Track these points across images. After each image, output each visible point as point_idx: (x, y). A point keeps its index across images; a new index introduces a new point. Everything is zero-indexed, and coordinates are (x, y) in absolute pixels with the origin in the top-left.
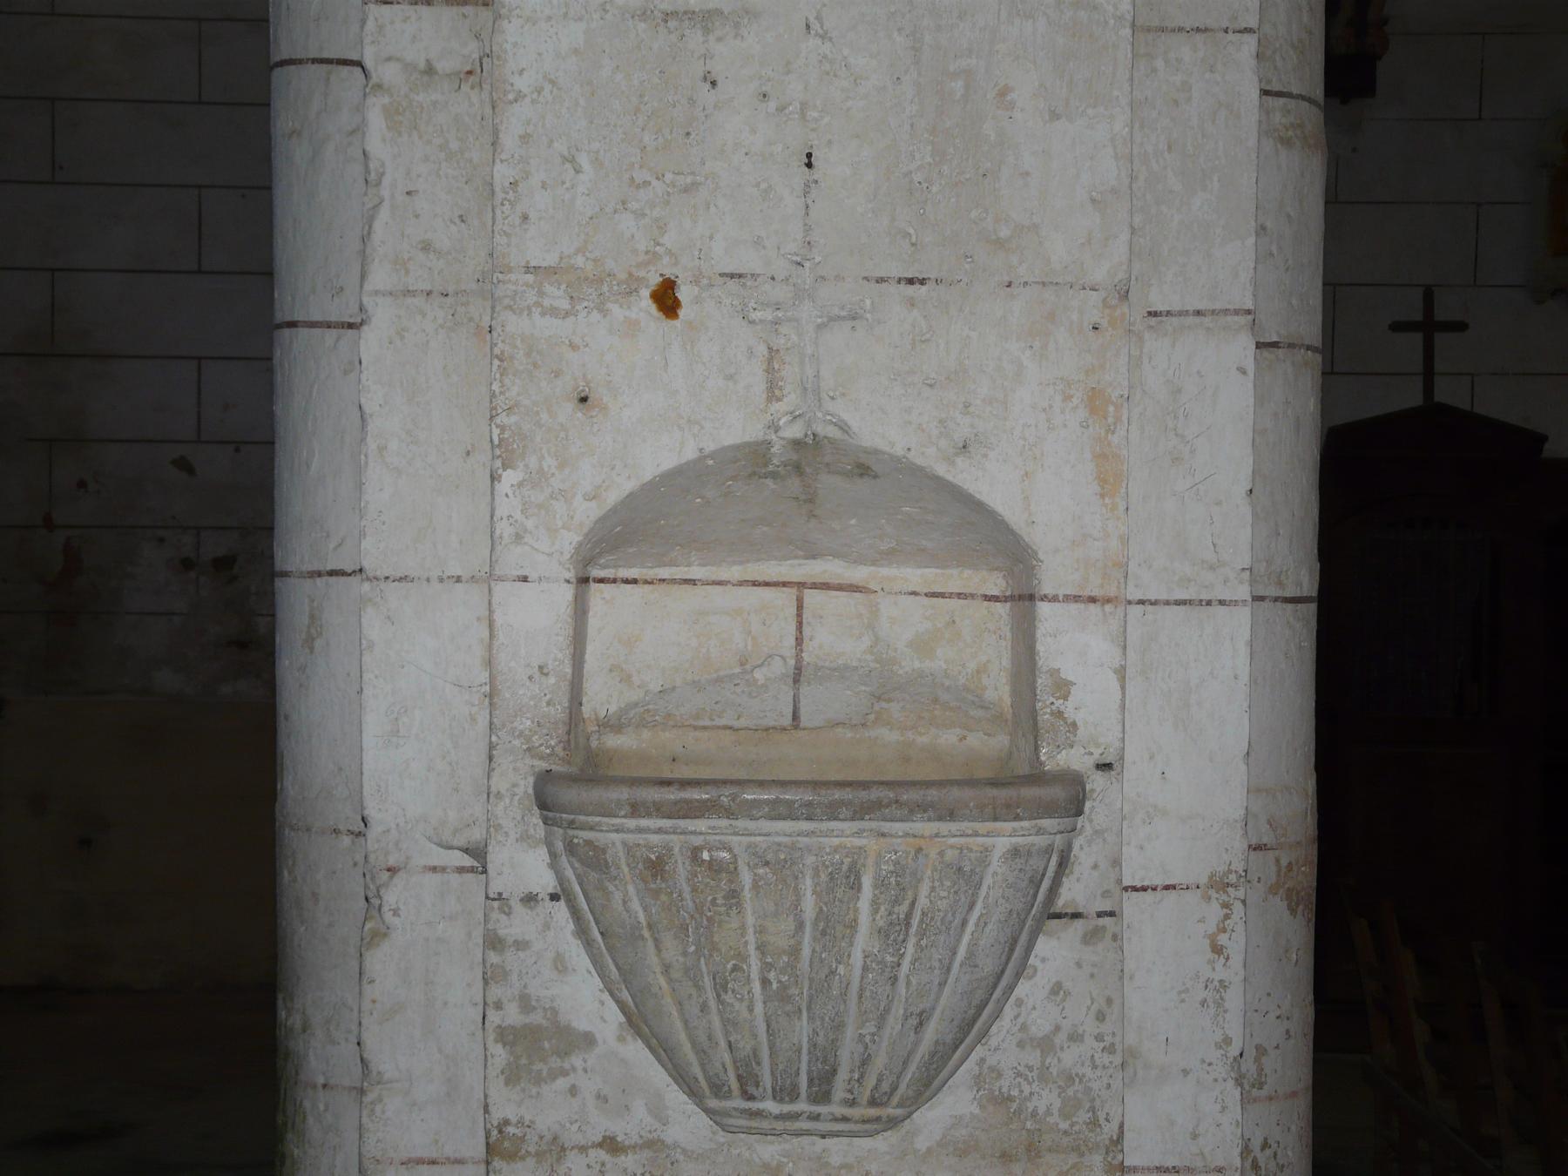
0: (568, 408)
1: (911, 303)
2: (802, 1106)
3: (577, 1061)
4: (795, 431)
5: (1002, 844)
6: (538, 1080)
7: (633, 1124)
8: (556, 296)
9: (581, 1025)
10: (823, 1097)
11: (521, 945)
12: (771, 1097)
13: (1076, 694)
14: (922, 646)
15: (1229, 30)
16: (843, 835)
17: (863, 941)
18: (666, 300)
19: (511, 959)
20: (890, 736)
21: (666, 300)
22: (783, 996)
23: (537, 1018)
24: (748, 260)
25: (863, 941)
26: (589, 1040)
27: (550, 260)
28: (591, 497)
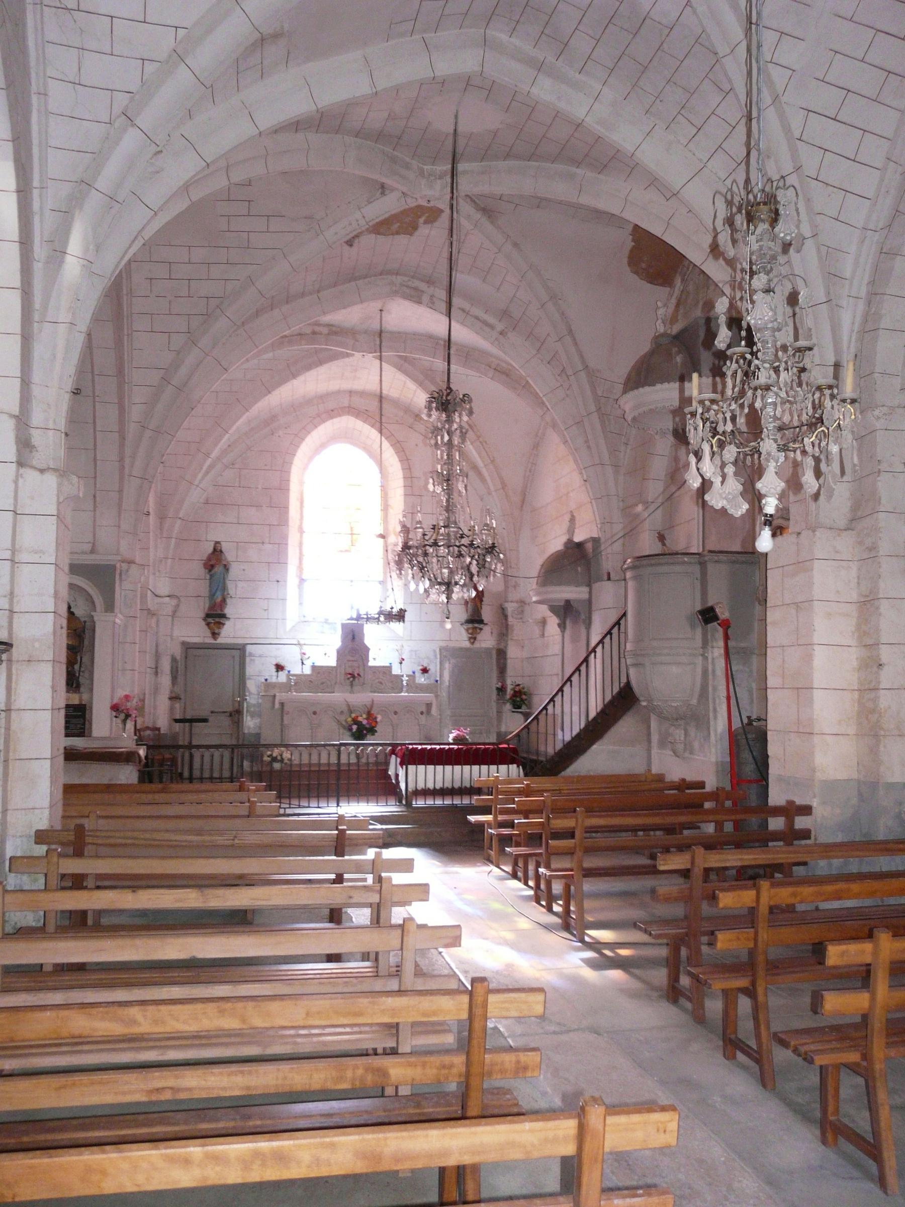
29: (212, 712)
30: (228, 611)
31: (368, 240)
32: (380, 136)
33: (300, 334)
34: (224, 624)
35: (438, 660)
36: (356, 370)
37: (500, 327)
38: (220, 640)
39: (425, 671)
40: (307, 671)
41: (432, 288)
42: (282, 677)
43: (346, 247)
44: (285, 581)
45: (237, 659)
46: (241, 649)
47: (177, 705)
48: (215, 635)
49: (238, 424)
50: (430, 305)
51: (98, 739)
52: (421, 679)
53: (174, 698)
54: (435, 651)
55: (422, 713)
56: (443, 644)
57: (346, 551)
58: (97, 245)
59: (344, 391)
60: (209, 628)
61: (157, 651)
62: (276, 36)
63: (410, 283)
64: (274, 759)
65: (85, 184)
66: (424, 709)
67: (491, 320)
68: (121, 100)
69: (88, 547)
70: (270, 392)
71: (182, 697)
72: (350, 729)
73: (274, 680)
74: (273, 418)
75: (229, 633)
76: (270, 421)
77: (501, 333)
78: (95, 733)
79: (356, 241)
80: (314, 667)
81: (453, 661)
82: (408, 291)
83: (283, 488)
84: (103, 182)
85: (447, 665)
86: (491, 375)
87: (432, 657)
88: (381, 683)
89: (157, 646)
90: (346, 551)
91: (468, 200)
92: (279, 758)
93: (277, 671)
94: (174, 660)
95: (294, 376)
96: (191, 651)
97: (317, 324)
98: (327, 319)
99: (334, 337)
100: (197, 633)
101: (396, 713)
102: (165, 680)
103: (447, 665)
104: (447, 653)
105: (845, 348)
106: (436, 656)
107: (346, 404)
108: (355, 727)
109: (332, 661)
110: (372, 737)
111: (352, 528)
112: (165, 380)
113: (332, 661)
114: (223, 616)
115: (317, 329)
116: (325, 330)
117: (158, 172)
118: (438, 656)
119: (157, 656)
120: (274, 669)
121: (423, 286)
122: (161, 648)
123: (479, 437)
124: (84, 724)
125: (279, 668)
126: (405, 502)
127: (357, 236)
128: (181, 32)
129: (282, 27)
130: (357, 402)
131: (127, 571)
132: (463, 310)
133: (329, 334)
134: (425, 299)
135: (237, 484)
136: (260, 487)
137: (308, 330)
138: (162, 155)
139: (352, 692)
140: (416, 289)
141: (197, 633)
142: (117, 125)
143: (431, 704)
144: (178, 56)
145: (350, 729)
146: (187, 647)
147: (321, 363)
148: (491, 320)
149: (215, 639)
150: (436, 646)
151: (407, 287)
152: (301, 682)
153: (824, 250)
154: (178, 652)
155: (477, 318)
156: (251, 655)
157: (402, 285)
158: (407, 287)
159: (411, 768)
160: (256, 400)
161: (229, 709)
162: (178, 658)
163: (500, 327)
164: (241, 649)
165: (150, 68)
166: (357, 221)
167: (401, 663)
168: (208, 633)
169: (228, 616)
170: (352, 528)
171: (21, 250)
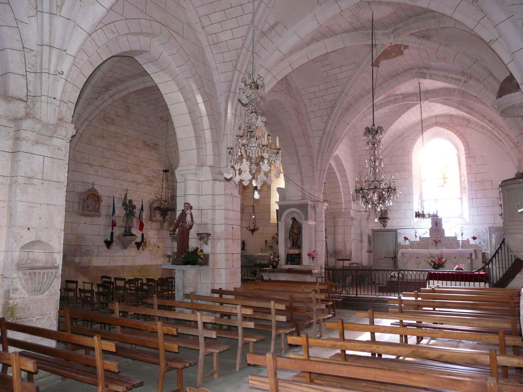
0: (20, 238)
1: (47, 230)
2: (38, 293)
3: (18, 291)
4: (37, 240)
5: (55, 271)
6: (15, 293)
7: (23, 296)
8: (20, 228)
9: (19, 288)
10: (40, 292)
11: (14, 282)
12: (313, 219)
13: (57, 260)
14: (38, 257)
15: (316, 301)
16: (44, 271)
17: (45, 279)
18: (29, 229)
19: (13, 283)
20: (33, 264)
21: (29, 229)
22: (39, 284)
23: (15, 288)
24: (35, 226)
25: (45, 279)
26: (19, 289)
27: (19, 225)
28: (22, 245)
29: (385, 257)
30: (389, 215)
34: (387, 221)
35: (488, 233)
36: (430, 108)
38: (386, 228)
39: (474, 238)
40: (418, 240)
41: (430, 71)
42: (407, 242)
44: (413, 202)
45: (394, 236)
46: (395, 231)
47: (371, 255)
48: (384, 226)
50: (430, 78)
51: (304, 266)
52: (472, 242)
53: (370, 252)
54: (486, 229)
55: (468, 258)
56: (491, 225)
57: (442, 186)
59: (433, 116)
60: (381, 223)
61: (361, 233)
63: (420, 71)
64: (392, 277)
66: (469, 256)
67: (458, 77)
69: (300, 198)
70: (392, 125)
71: (373, 251)
72: (431, 265)
73: (404, 244)
75: (391, 224)
77: (465, 82)
78: (304, 264)
80: (420, 238)
81: (496, 233)
82: (420, 75)
83: (409, 163)
85: (493, 235)
86: (474, 100)
87: (485, 232)
88: (451, 244)
89: (361, 231)
90: (442, 186)
91: (413, 36)
92: (393, 276)
93: (405, 240)
94: (369, 236)
96: (375, 233)
99: (406, 98)
100: (379, 227)
101: (455, 258)
102: (365, 245)
103: (493, 235)
104: (492, 230)
106: (487, 231)
107: (435, 122)
108: (432, 264)
109: (428, 235)
110: (443, 268)
111: (444, 176)
112: (324, 133)
113: (428, 235)
114: (387, 218)
115: (397, 97)
118: (488, 232)
119: (361, 235)
120: (404, 239)
121: (425, 71)
122: (363, 232)
124: (299, 260)
125: (406, 239)
126: (466, 161)
129: (276, 21)
130: (440, 120)
131: (317, 205)
134: (428, 76)
135: (390, 164)
136: (399, 163)
139: (436, 248)
140: (422, 73)
141: (379, 227)
143: (472, 254)
145: (431, 265)
146: (374, 231)
147: (408, 109)
148: (458, 77)
149: (385, 228)
150: (487, 227)
151: (419, 73)
152: (413, 245)
154: (371, 234)
155: (452, 78)
156: (400, 233)
157: (416, 73)
158: (419, 73)
159: (430, 281)
161: (392, 256)
162: (371, 235)
163: (463, 79)
164: (395, 231)
165: (238, 51)
167: (462, 235)
168: (382, 225)
169: (389, 218)
170: (444, 176)
171: (227, 111)
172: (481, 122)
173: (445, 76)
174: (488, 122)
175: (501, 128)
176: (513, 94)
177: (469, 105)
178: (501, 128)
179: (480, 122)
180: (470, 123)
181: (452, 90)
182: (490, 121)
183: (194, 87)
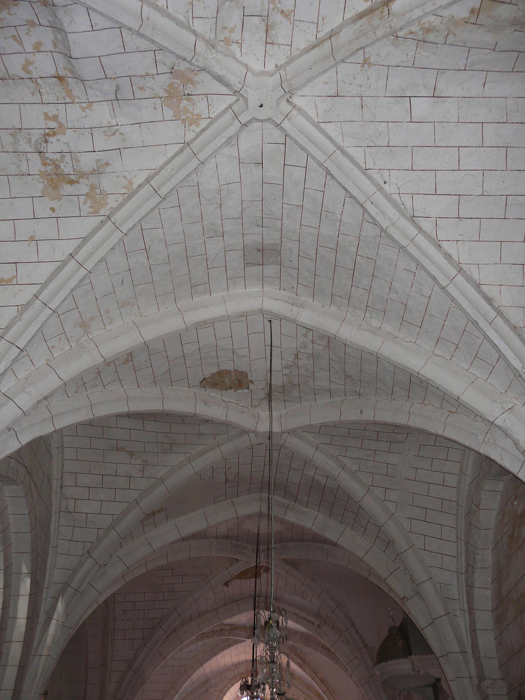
31: (237, 582)
32: (227, 537)
33: (213, 631)
37: (317, 622)
43: (225, 588)
49: (185, 685)
58: (67, 612)
62: (159, 511)
65: (67, 585)
68: (88, 545)
74: (208, 680)
76: (206, 682)
79: (230, 583)
84: (74, 584)
95: (215, 654)
97: (223, 624)
98: (228, 621)
105: (466, 642)
115: (223, 627)
116: (228, 628)
117: (104, 574)
123: (328, 689)
127: (230, 581)
128: (115, 516)
129: (162, 507)
132: (296, 614)
133: (230, 630)
137: (218, 628)
138: (107, 565)
142: (84, 557)
144: (112, 526)
147: (229, 646)
153: (438, 585)
155: (304, 618)
160: (195, 670)
163: (317, 622)
165: (101, 532)
166: (226, 575)
172: (312, 681)
173: (296, 614)
174: (319, 680)
175: (332, 693)
176: (400, 660)
177: (301, 654)
178: (332, 693)
179: (311, 679)
180: (294, 678)
181: (293, 631)
182: (322, 682)
183: (25, 569)
